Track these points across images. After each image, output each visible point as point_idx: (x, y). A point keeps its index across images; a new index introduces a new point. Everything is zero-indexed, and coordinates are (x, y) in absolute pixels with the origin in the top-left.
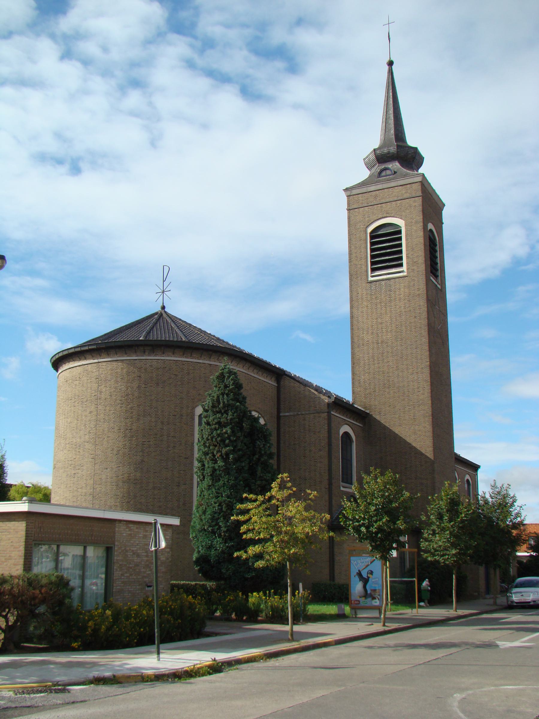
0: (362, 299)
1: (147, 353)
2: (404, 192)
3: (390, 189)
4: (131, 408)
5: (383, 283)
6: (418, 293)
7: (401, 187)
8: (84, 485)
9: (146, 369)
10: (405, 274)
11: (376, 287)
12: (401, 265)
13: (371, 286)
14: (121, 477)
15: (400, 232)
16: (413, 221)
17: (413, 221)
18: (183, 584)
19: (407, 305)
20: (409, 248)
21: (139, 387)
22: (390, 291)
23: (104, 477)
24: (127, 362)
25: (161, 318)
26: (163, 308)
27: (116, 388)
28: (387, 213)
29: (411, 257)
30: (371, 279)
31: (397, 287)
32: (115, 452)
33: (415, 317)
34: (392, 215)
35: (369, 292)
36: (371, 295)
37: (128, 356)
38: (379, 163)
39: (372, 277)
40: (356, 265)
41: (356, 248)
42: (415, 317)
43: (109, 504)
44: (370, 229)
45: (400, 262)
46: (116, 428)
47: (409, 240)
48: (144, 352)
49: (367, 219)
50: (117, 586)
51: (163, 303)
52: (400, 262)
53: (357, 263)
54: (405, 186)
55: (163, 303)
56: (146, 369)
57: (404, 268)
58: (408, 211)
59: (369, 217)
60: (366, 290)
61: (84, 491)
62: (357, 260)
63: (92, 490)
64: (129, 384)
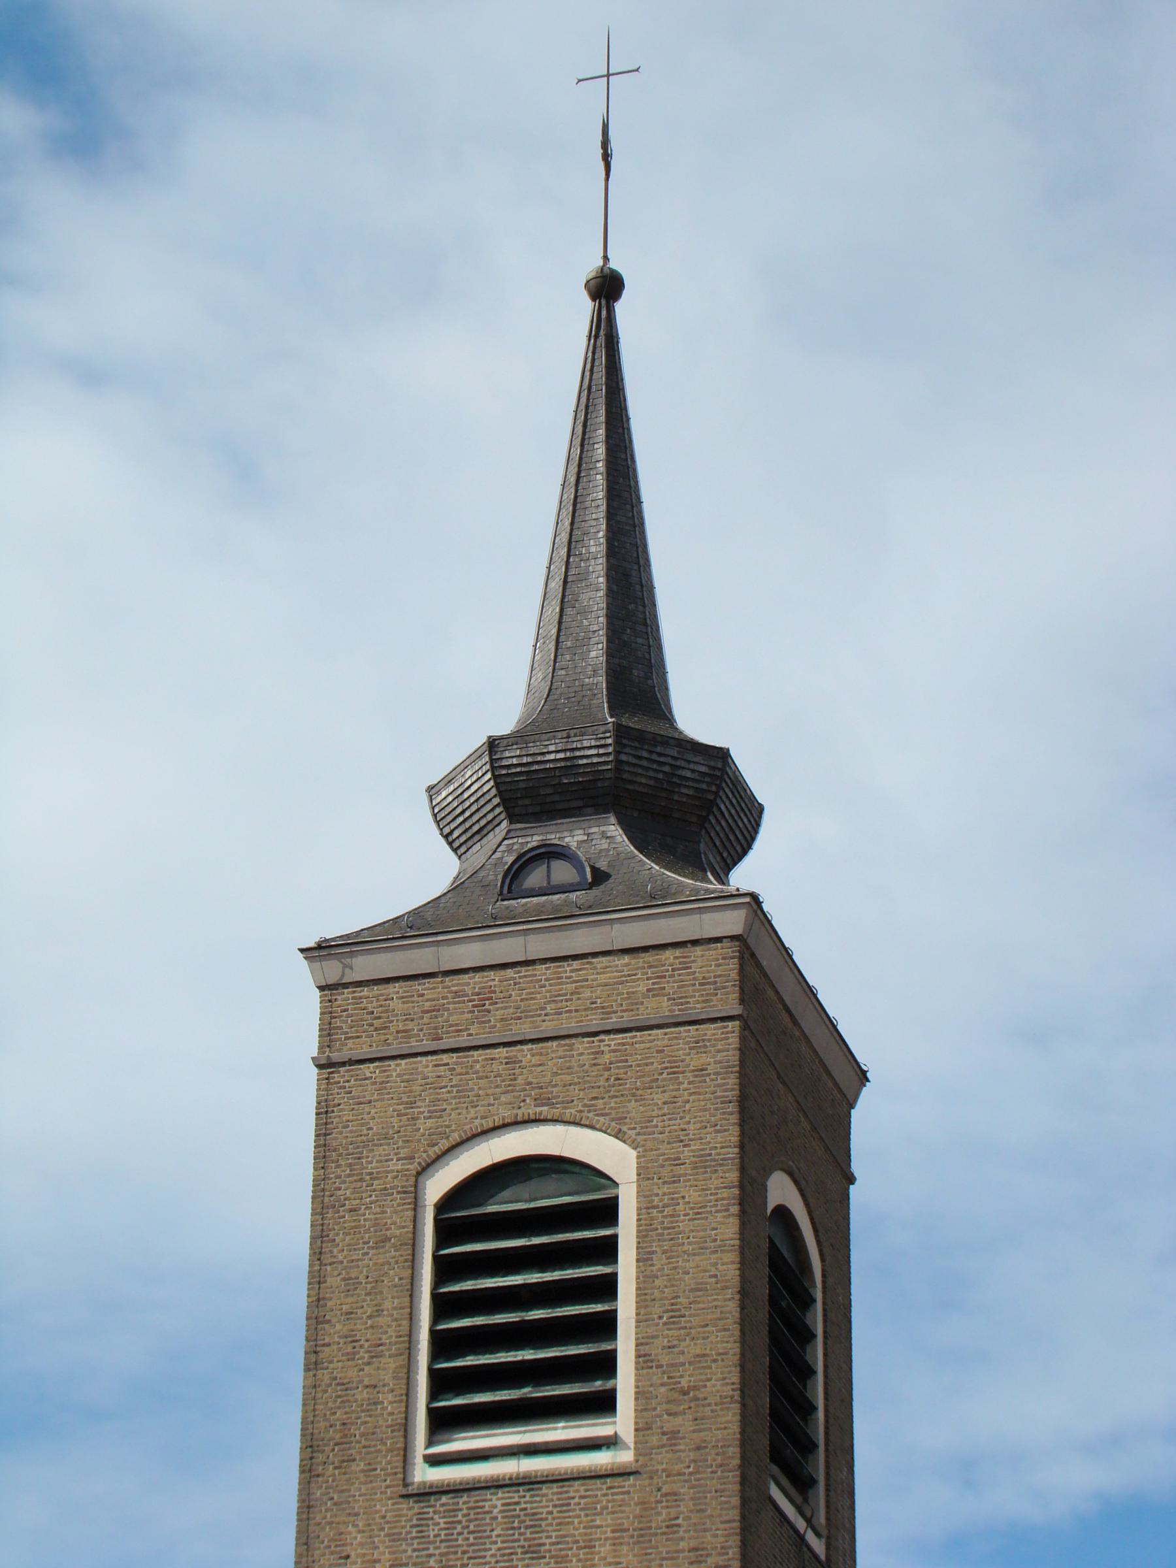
3: (567, 967)
7: (626, 959)
10: (625, 1457)
11: (451, 1525)
12: (605, 1404)
13: (422, 1522)
15: (608, 1211)
28: (539, 1101)
30: (425, 1474)
34: (569, 1113)
39: (435, 1461)
40: (345, 1386)
41: (351, 1285)
47: (659, 1261)
49: (424, 1125)
57: (623, 1421)
58: (659, 1098)
60: (395, 1538)
62: (351, 1357)
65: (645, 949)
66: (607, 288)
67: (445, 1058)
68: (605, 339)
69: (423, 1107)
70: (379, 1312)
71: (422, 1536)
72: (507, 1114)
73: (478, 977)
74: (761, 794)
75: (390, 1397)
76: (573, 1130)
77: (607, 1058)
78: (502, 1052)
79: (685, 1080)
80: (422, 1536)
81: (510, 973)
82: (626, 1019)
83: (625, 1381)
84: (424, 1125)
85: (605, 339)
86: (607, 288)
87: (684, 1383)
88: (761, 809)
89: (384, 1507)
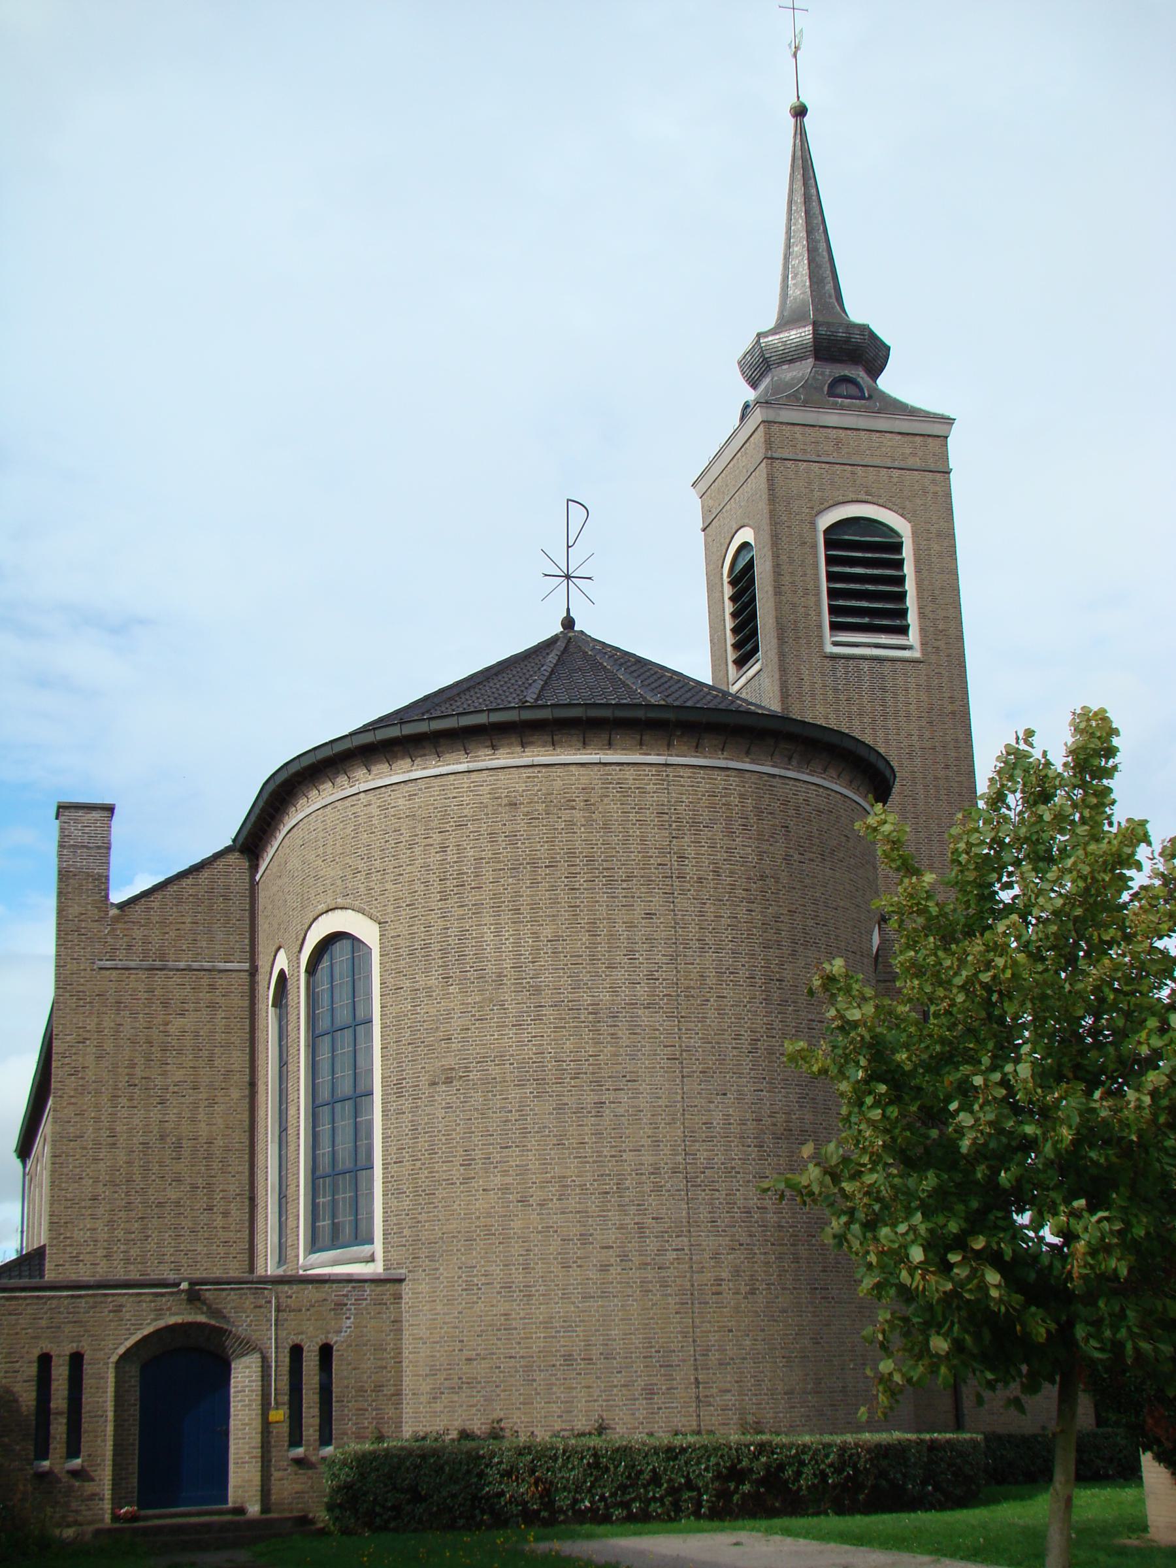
0: (813, 695)
1: (794, 763)
2: (908, 451)
3: (875, 436)
4: (777, 918)
5: (865, 665)
6: (950, 708)
7: (899, 437)
8: (646, 1142)
9: (797, 808)
10: (916, 654)
11: (847, 673)
12: (903, 630)
13: (834, 670)
14: (767, 1121)
15: (897, 547)
16: (933, 529)
17: (933, 529)
18: (948, 1441)
19: (927, 735)
20: (926, 594)
21: (787, 858)
22: (884, 689)
23: (717, 1118)
24: (754, 777)
25: (569, 648)
26: (568, 623)
27: (729, 850)
28: (867, 493)
29: (931, 615)
30: (830, 649)
31: (900, 681)
32: (746, 1046)
33: (947, 767)
34: (881, 501)
35: (829, 681)
36: (836, 690)
37: (753, 762)
38: (817, 358)
39: (836, 644)
40: (794, 605)
41: (791, 561)
42: (947, 767)
43: (740, 1203)
44: (826, 520)
45: (898, 622)
46: (743, 973)
47: (925, 573)
48: (790, 758)
49: (817, 494)
50: (275, 1487)
51: (568, 610)
52: (898, 622)
53: (796, 600)
54: (910, 438)
55: (568, 610)
56: (797, 808)
57: (914, 637)
58: (919, 502)
59: (820, 490)
60: (823, 674)
61: (648, 1158)
62: (795, 592)
63: (680, 1158)
64: (765, 847)
65: (908, 434)
66: (800, 112)
67: (823, 465)
68: (801, 134)
69: (815, 486)
70: (805, 575)
71: (834, 675)
72: (851, 496)
73: (835, 431)
74: (888, 343)
75: (1131, 1095)
76: (882, 509)
77: (895, 480)
78: (849, 468)
79: (930, 496)
80: (834, 675)
81: (849, 432)
82: (902, 465)
83: (912, 618)
84: (817, 494)
85: (801, 134)
86: (800, 112)
87: (940, 627)
88: (888, 349)
89: (816, 660)
